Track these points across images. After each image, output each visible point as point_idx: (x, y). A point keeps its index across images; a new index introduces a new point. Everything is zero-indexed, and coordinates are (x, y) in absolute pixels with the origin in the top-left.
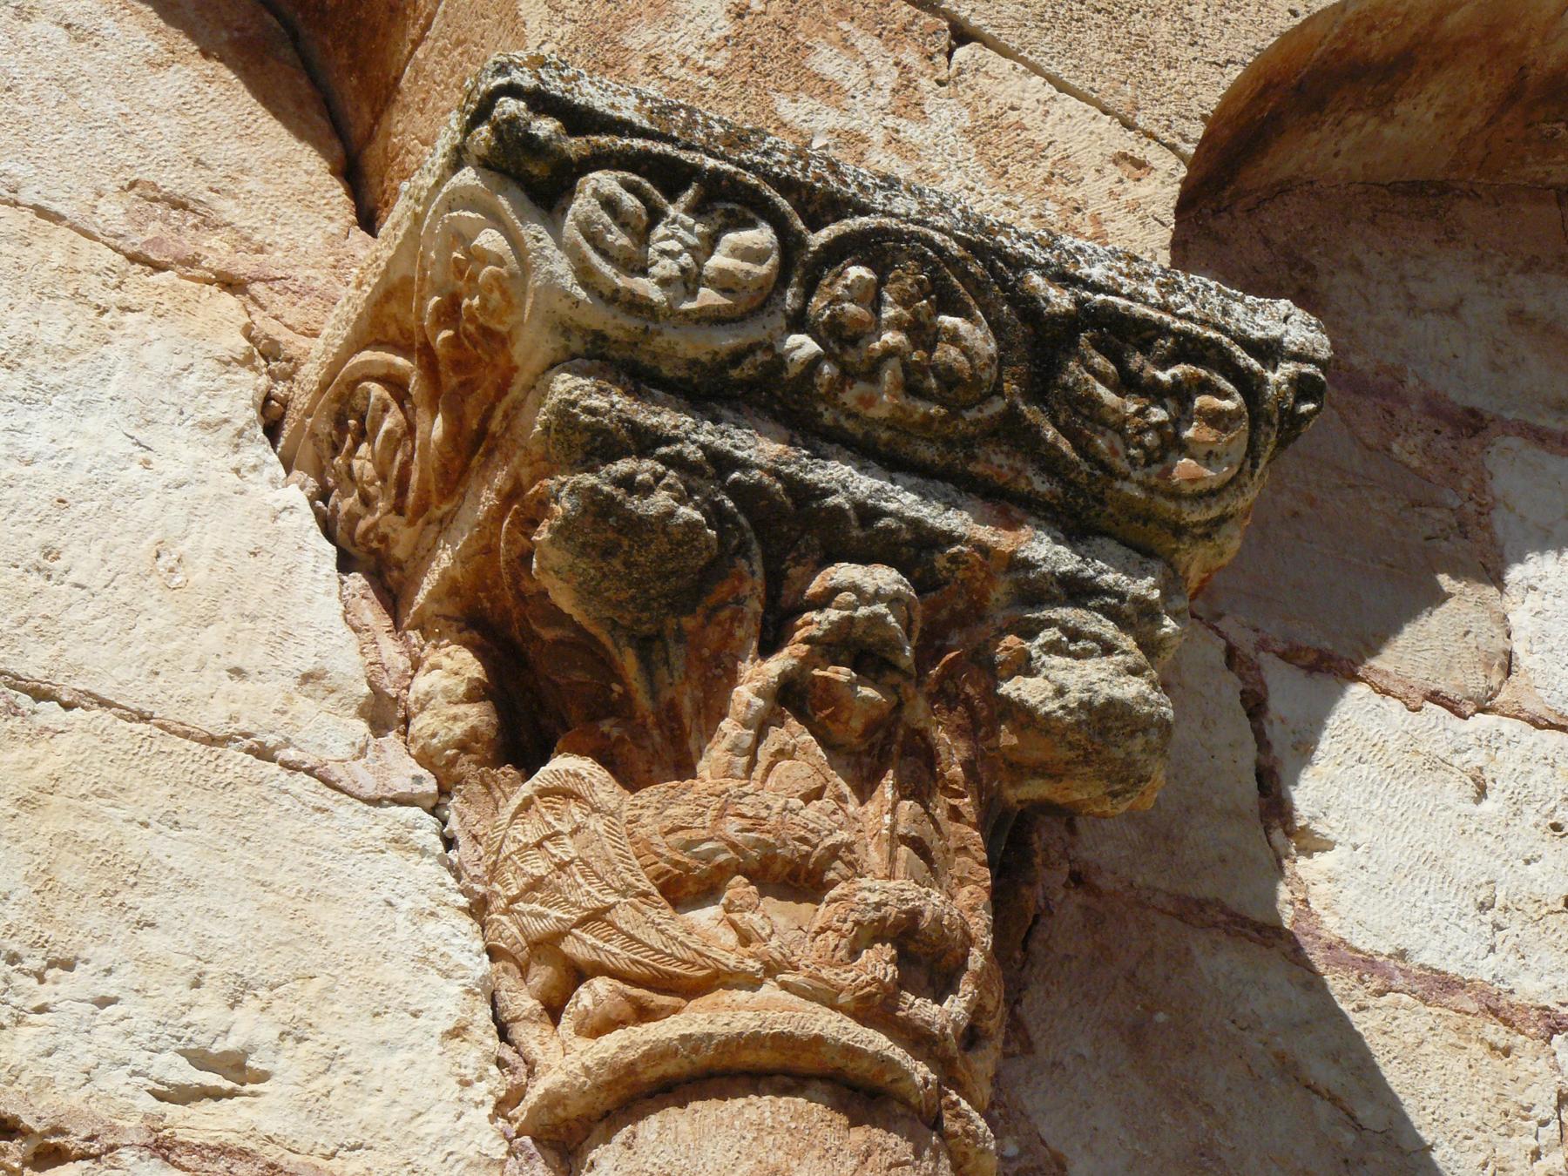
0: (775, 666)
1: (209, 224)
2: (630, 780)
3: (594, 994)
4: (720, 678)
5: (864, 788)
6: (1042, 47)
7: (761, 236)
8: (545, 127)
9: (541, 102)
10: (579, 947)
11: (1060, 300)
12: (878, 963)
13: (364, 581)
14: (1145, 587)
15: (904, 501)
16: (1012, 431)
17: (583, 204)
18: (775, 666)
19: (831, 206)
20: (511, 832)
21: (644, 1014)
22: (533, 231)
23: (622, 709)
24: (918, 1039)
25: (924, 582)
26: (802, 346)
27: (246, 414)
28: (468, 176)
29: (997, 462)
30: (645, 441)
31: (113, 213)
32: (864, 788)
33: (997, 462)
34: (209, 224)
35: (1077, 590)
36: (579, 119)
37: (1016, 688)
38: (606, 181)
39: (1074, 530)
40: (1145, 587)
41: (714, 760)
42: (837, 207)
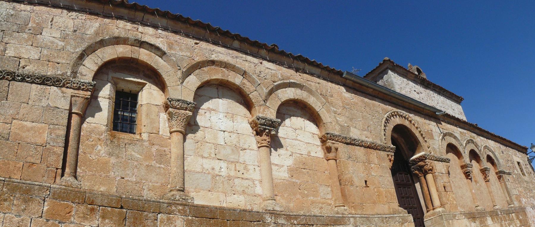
0: (265, 133)
1: (246, 115)
2: (261, 137)
3: (260, 143)
4: (263, 134)
5: (267, 136)
6: (272, 108)
7: (265, 120)
8: (259, 118)
9: (259, 117)
10: (259, 142)
11: (273, 121)
12: (268, 143)
13: (66, 11)
14: (275, 129)
15: (268, 128)
16: (272, 125)
17: (260, 120)
18: (265, 133)
19: (266, 119)
20: (8, 88)
21: (261, 144)
22: (258, 121)
23: (260, 134)
24: (268, 145)
25: (269, 130)
26: (266, 123)
27: (248, 122)
28: (256, 119)
29: (271, 126)
30: (261, 127)
31: (243, 116)
32: (267, 136)
33: (271, 126)
34: (246, 115)
35: (273, 130)
36: (260, 117)
37: (271, 133)
38: (260, 119)
39: (273, 128)
40: (275, 129)
41: (263, 136)
42: (267, 119)
